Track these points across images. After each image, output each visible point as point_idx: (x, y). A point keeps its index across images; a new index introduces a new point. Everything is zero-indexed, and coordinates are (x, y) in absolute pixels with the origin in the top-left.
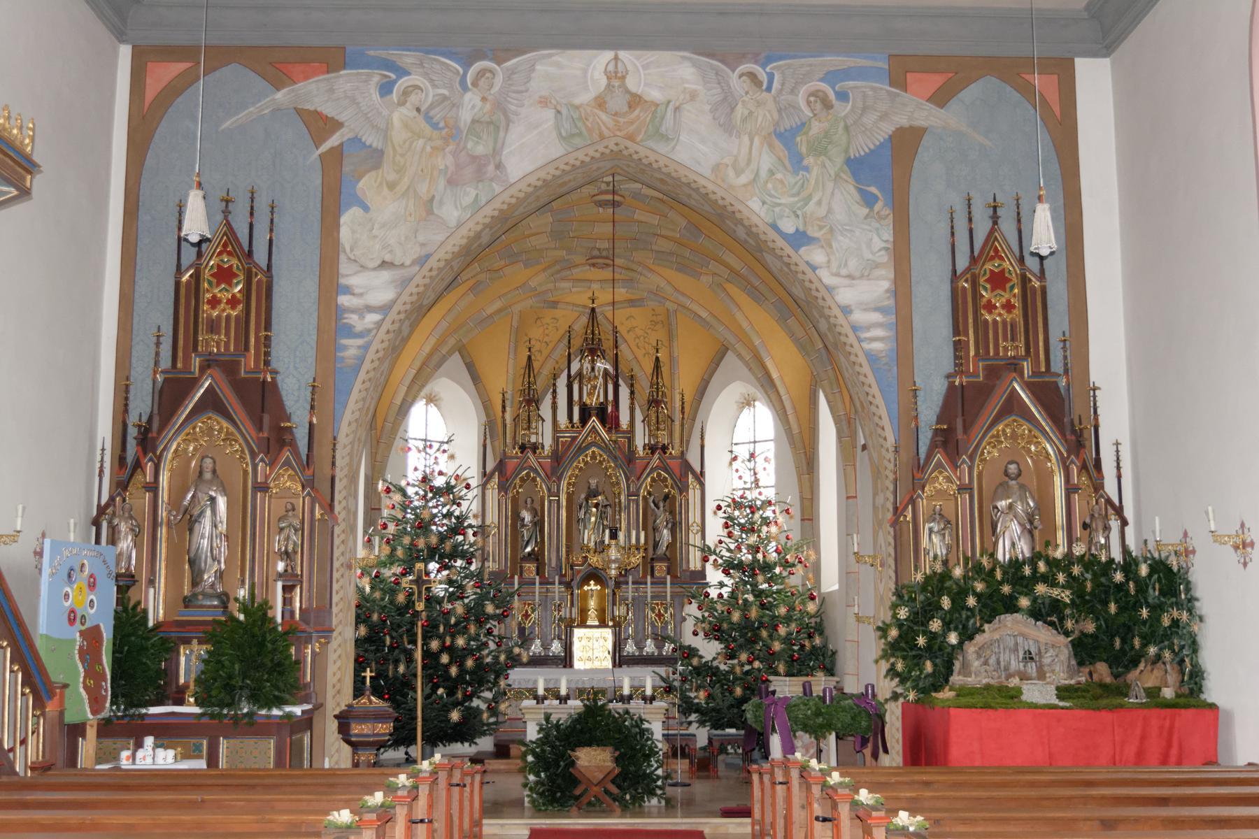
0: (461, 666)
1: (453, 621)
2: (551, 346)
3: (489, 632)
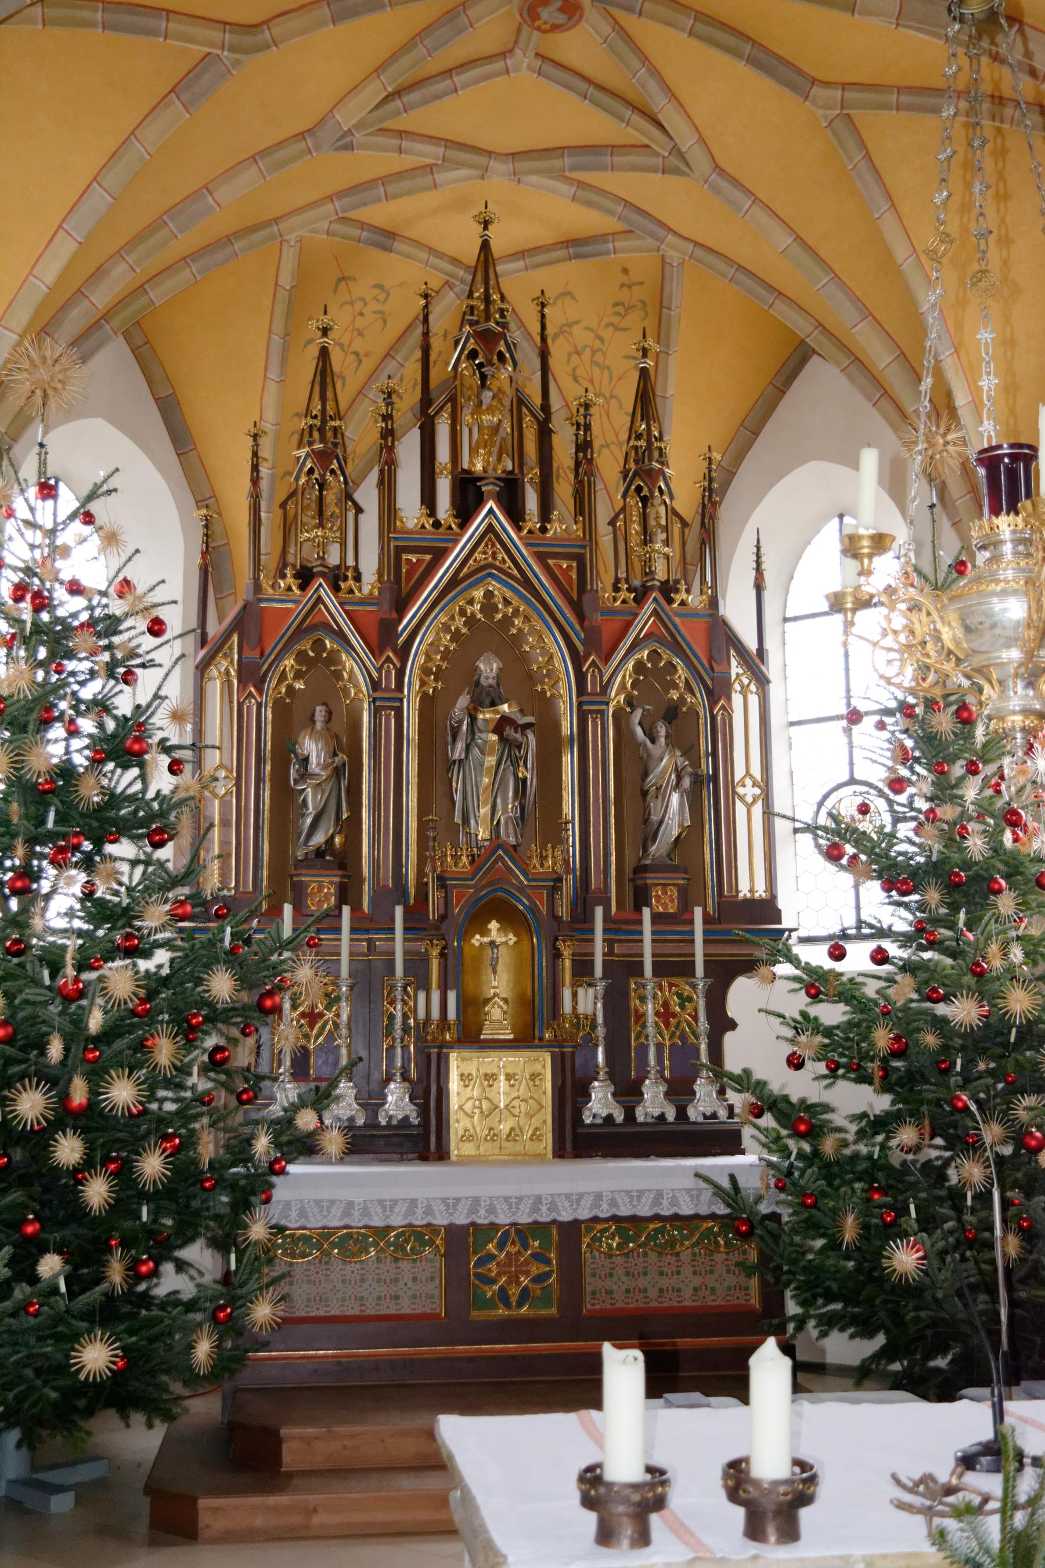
0: (124, 1176)
1: (95, 1022)
2: (368, 365)
3: (217, 1061)
